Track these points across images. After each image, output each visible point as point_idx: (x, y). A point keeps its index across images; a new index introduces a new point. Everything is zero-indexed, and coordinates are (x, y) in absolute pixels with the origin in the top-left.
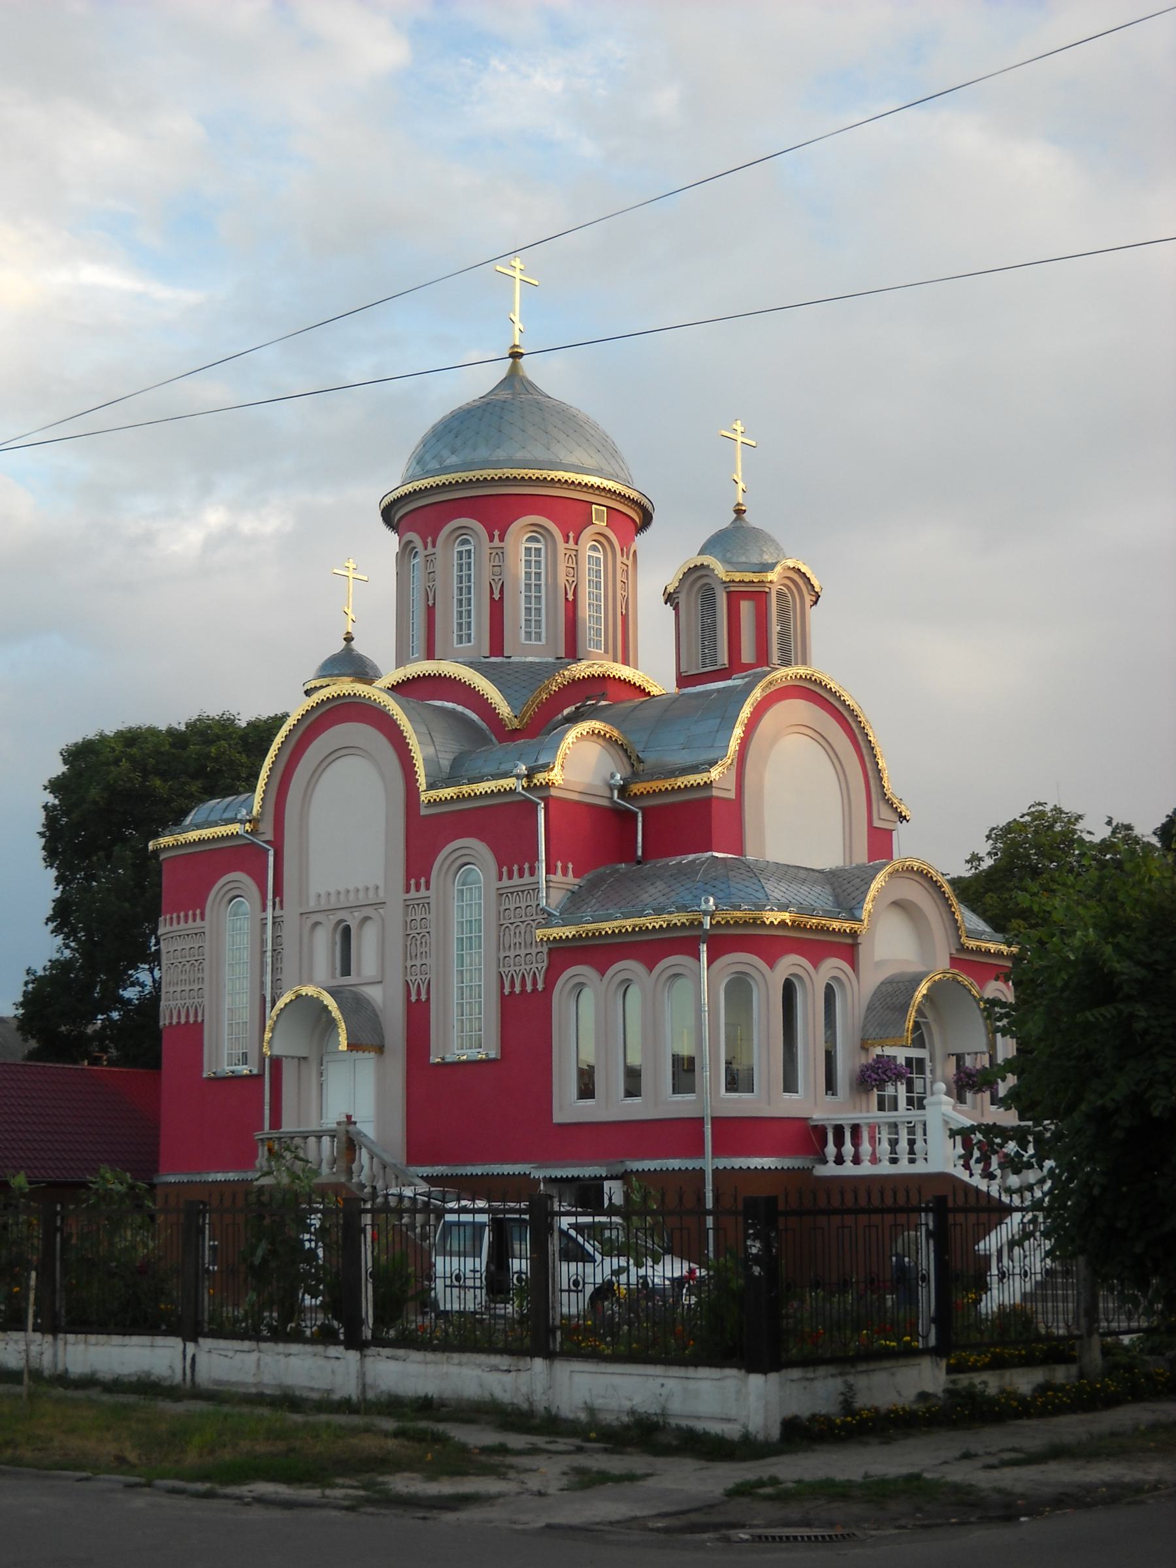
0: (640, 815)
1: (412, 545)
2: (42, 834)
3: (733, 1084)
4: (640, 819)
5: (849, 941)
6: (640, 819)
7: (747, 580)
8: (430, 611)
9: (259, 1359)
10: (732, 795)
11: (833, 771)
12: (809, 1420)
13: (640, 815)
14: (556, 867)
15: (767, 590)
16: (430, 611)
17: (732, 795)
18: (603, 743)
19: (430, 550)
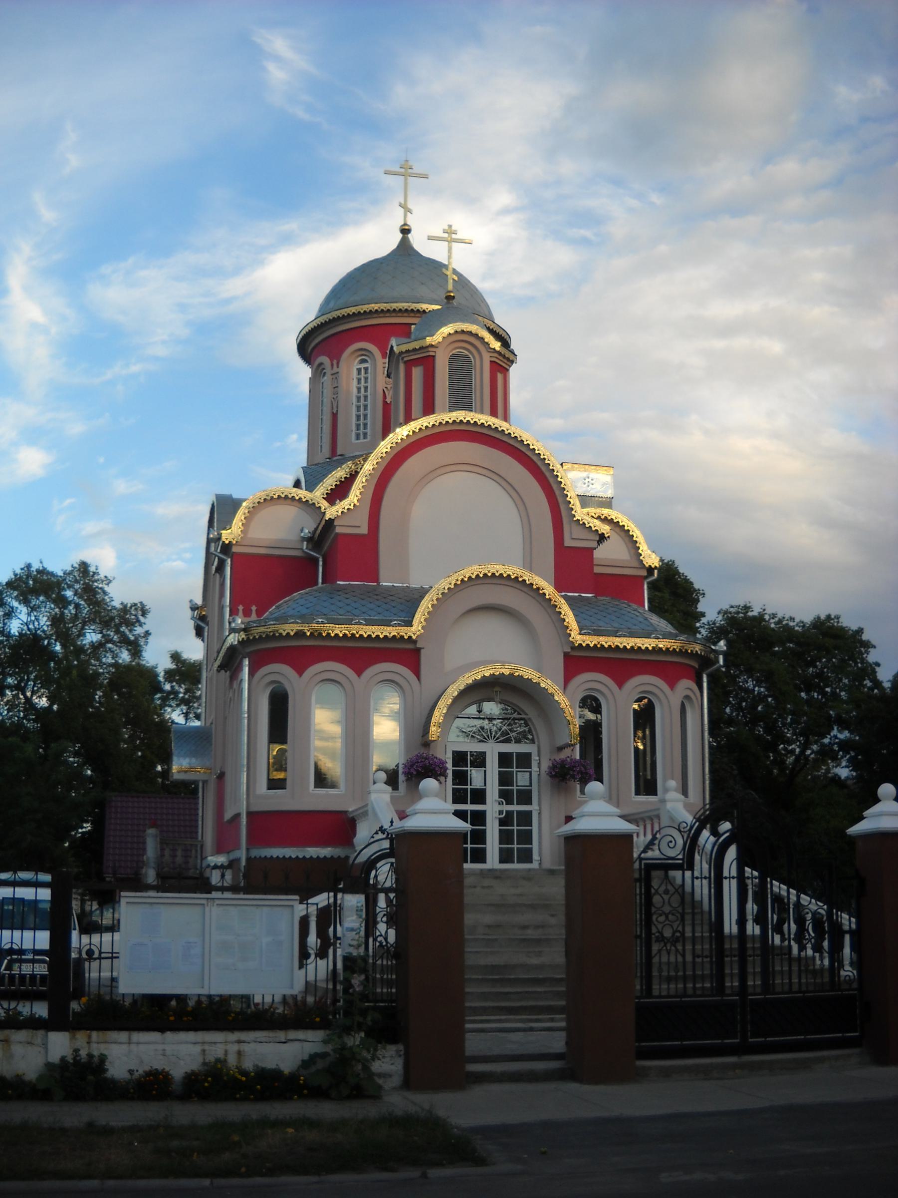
0: (321, 559)
1: (322, 367)
2: (860, 631)
3: (275, 784)
4: (321, 563)
5: (411, 646)
6: (321, 563)
7: (411, 349)
8: (335, 416)
9: (204, 1051)
10: (364, 530)
11: (510, 499)
12: (37, 1079)
13: (321, 559)
14: (251, 610)
15: (432, 354)
16: (335, 416)
17: (364, 530)
18: (299, 505)
19: (335, 370)
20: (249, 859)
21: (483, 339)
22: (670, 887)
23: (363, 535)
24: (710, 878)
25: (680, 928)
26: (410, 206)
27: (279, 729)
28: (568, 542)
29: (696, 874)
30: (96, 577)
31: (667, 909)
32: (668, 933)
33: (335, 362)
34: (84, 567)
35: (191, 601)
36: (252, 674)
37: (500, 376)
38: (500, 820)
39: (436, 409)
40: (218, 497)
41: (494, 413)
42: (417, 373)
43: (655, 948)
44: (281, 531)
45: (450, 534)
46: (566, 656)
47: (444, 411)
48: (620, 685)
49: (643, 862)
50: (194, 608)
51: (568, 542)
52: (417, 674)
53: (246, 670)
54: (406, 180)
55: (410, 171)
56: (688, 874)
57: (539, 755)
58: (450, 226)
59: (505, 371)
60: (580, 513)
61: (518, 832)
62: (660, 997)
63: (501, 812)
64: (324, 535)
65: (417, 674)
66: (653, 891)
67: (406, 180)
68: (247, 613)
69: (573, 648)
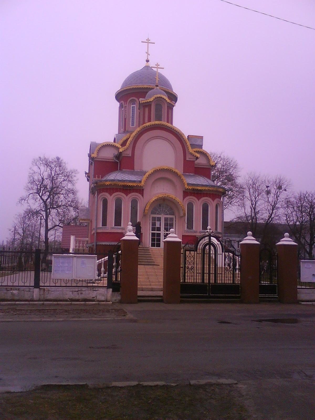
4: (119, 164)
6: (119, 164)
10: (130, 155)
17: (130, 155)
20: (96, 245)
21: (165, 99)
22: (191, 255)
23: (130, 157)
24: (183, 254)
25: (193, 266)
26: (149, 53)
27: (72, 226)
28: (187, 159)
29: (198, 252)
30: (47, 182)
31: (190, 261)
32: (190, 266)
33: (126, 103)
34: (58, 159)
35: (85, 172)
36: (98, 195)
37: (170, 111)
38: (164, 236)
39: (151, 121)
40: (91, 142)
41: (168, 122)
42: (147, 110)
43: (186, 270)
44: (109, 155)
45: (156, 155)
46: (184, 192)
47: (154, 121)
48: (199, 200)
49: (184, 249)
50: (86, 173)
51: (187, 159)
52: (143, 196)
53: (96, 193)
54: (148, 44)
55: (149, 41)
56: (196, 252)
57: (175, 218)
58: (157, 63)
59: (172, 109)
60: (191, 150)
61: (156, 241)
62: (228, 284)
63: (165, 234)
64: (119, 156)
65: (143, 196)
66: (186, 256)
67: (148, 44)
68: (98, 177)
69: (186, 189)
